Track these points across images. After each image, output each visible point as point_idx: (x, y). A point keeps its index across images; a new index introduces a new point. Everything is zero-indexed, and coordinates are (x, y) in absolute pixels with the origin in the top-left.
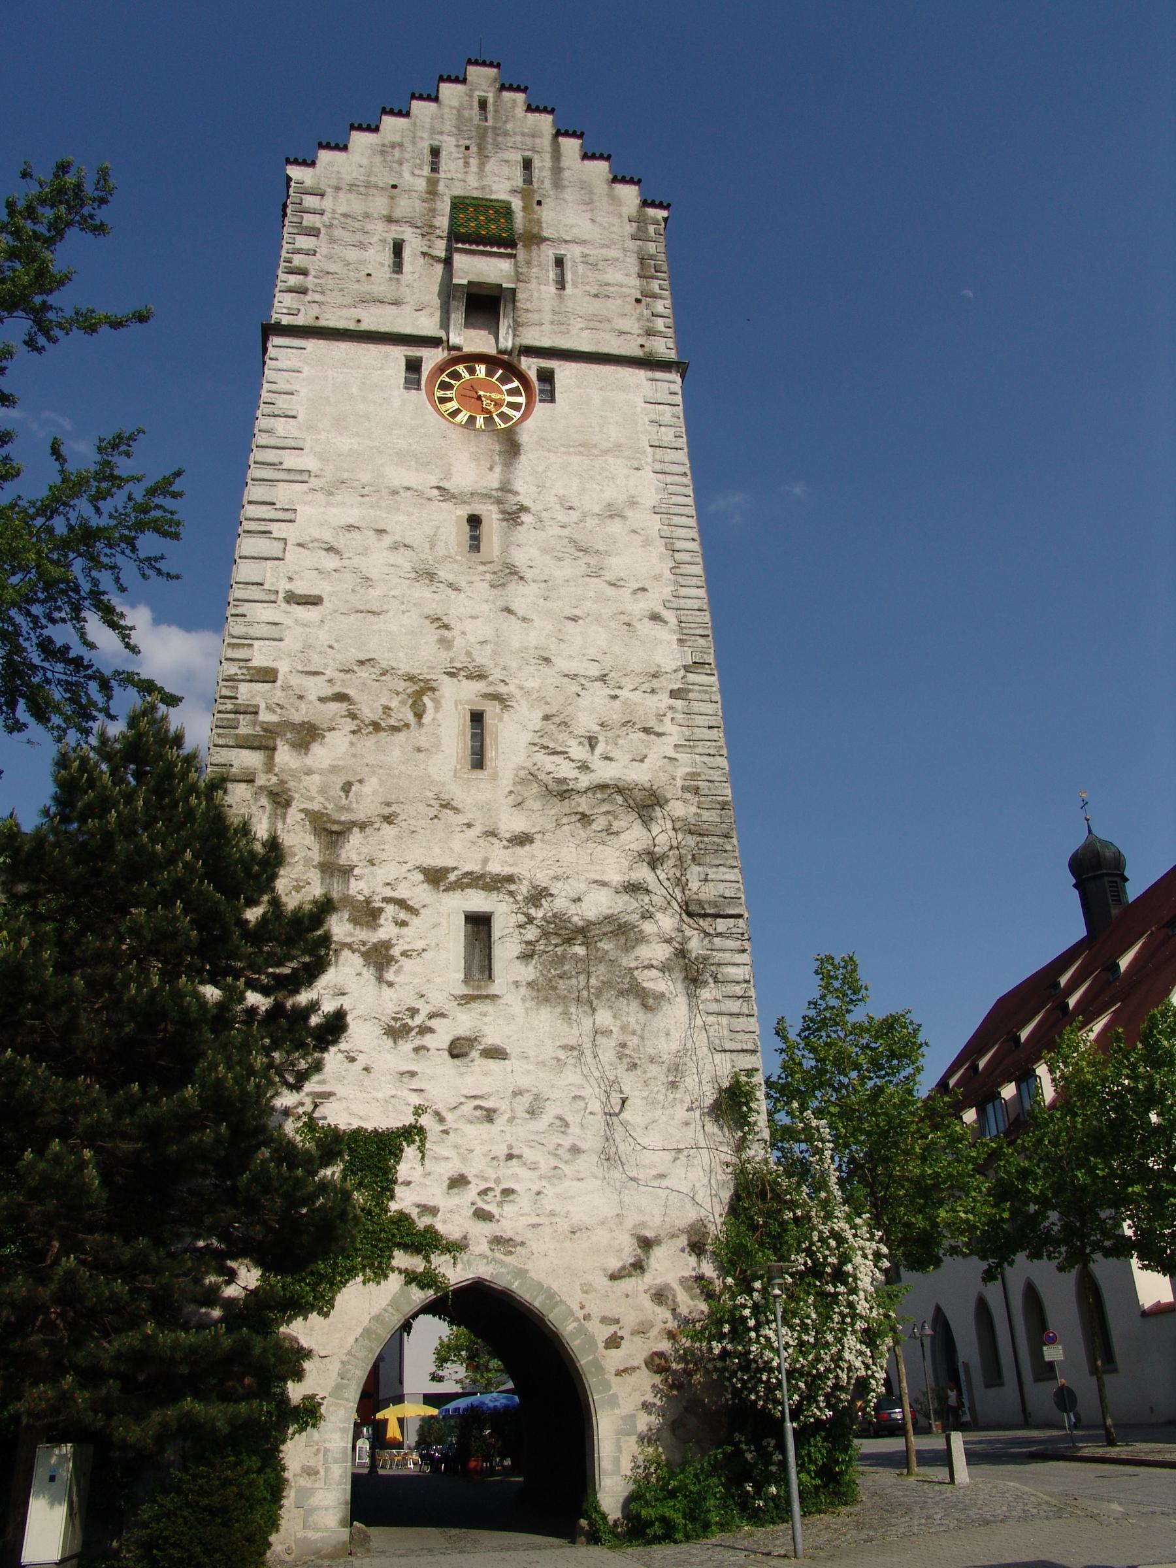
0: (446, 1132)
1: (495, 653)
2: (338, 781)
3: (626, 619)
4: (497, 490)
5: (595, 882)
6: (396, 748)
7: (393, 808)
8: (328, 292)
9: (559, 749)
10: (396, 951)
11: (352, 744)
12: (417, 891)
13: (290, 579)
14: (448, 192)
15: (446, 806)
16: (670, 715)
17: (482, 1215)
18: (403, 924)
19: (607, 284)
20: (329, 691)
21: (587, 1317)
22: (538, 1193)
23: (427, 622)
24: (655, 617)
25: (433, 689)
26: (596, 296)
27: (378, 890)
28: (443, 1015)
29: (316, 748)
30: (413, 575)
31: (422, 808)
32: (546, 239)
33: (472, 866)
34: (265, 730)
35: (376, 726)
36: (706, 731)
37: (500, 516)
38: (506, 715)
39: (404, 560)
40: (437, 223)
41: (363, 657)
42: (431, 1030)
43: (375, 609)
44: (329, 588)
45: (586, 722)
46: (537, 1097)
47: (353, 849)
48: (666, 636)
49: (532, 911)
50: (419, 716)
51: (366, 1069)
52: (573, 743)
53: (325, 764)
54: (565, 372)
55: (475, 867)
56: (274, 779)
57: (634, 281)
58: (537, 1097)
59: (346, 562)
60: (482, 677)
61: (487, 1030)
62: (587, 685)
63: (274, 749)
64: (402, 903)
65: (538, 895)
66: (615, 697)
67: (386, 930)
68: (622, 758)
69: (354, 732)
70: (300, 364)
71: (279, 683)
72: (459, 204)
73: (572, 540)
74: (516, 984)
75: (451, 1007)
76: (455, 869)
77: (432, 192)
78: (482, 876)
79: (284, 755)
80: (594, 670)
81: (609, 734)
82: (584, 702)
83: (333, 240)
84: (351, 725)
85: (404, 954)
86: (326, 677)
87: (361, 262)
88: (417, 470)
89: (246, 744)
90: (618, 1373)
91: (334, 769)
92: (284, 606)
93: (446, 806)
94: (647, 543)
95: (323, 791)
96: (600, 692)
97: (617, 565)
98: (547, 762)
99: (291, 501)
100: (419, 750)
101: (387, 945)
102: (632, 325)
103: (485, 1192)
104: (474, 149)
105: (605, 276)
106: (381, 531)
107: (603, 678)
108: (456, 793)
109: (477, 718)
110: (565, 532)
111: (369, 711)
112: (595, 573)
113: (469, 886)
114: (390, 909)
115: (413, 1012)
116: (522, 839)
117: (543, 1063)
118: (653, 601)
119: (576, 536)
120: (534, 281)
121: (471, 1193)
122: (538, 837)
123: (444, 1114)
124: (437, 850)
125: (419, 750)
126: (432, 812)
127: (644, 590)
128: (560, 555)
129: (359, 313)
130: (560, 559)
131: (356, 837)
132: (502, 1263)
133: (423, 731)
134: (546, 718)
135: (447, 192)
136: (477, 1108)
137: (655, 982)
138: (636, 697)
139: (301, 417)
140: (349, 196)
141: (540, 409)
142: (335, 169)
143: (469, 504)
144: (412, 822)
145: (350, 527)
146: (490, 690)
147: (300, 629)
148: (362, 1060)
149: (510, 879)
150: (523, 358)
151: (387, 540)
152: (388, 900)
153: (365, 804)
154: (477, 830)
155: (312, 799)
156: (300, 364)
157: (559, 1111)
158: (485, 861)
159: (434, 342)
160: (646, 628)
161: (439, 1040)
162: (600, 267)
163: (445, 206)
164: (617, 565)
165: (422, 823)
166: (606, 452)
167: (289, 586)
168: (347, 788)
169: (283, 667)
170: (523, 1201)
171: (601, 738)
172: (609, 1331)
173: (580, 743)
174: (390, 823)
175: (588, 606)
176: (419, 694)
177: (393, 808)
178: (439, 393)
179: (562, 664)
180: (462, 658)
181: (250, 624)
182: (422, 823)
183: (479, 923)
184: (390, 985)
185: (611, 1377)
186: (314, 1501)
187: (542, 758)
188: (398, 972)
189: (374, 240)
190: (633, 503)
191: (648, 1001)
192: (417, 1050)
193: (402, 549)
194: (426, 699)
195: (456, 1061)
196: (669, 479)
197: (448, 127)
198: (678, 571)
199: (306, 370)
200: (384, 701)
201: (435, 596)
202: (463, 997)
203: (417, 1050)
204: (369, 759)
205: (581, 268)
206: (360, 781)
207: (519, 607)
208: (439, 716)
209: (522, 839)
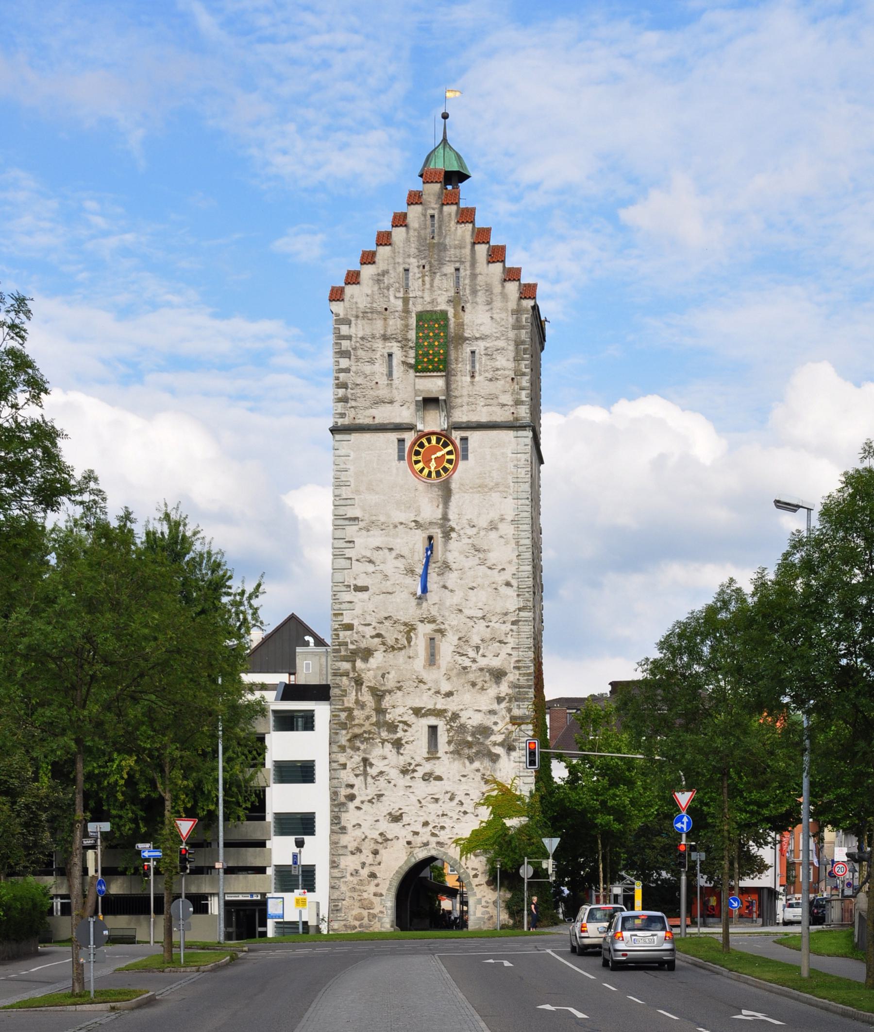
0: (421, 807)
1: (439, 609)
2: (380, 673)
3: (494, 586)
4: (440, 519)
5: (476, 710)
6: (401, 656)
7: (401, 684)
8: (358, 399)
9: (465, 653)
10: (403, 742)
11: (384, 656)
12: (410, 718)
13: (355, 579)
14: (416, 308)
15: (421, 681)
16: (511, 633)
17: (433, 835)
18: (406, 731)
19: (498, 369)
20: (374, 633)
21: (467, 868)
22: (453, 827)
23: (411, 596)
24: (508, 584)
25: (415, 629)
26: (491, 380)
27: (397, 718)
28: (421, 765)
29: (371, 660)
30: (405, 572)
31: (411, 682)
32: (467, 339)
33: (430, 706)
34: (351, 653)
35: (392, 647)
36: (526, 640)
37: (441, 535)
38: (443, 639)
39: (400, 563)
40: (409, 337)
41: (386, 616)
42: (416, 771)
43: (391, 591)
44: (371, 582)
45: (475, 640)
46: (453, 794)
47: (387, 702)
48: (511, 592)
49: (452, 724)
50: (409, 642)
51: (395, 785)
52: (470, 650)
53: (374, 666)
54: (474, 437)
55: (431, 706)
56: (356, 674)
57: (511, 365)
58: (453, 794)
59: (377, 568)
60: (434, 621)
61: (436, 770)
62: (477, 621)
63: (355, 661)
64: (405, 723)
65: (455, 716)
66: (488, 627)
67: (400, 734)
68: (490, 655)
69: (384, 651)
70: (349, 451)
71: (355, 630)
72: (420, 316)
73: (473, 545)
74: (446, 753)
75: (423, 762)
76: (424, 708)
77: (406, 311)
78: (434, 710)
79: (359, 664)
80: (480, 614)
81: (485, 645)
82: (474, 630)
83: (358, 360)
84: (383, 648)
85: (406, 743)
86: (372, 626)
87: (373, 374)
88: (405, 512)
89: (345, 659)
90: (477, 886)
91: (378, 668)
92: (353, 592)
93: (421, 681)
94: (507, 543)
95: (375, 677)
96: (483, 623)
97: (493, 557)
98: (460, 659)
99: (352, 537)
100: (410, 657)
101: (400, 739)
102: (507, 399)
103: (434, 827)
104: (427, 268)
105: (497, 363)
106: (391, 549)
107: (483, 618)
108: (425, 675)
109: (432, 639)
110: (470, 541)
111: (390, 642)
112: (482, 563)
113: (430, 715)
114: (401, 725)
115: (410, 764)
116: (449, 694)
117: (454, 782)
118: (507, 576)
119: (475, 543)
120: (459, 374)
121: (430, 827)
122: (455, 693)
123: (421, 800)
124: (417, 701)
125: (410, 657)
126: (415, 685)
127: (504, 569)
128: (467, 554)
129: (373, 412)
130: (467, 557)
131: (387, 698)
132: (440, 851)
133: (412, 648)
134: (460, 639)
135: (414, 308)
136: (432, 798)
137: (498, 750)
138: (497, 625)
139: (352, 485)
140: (363, 321)
141: (462, 464)
142: (355, 300)
143: (427, 529)
144: (408, 689)
145: (378, 548)
146: (437, 627)
147: (361, 604)
148: (393, 782)
149: (445, 711)
150: (453, 432)
151: (394, 554)
152: (400, 722)
153: (390, 682)
154: (433, 691)
155: (370, 681)
156: (349, 451)
157: (460, 799)
158: (435, 704)
159: (410, 428)
160: (504, 590)
161: (419, 774)
162: (494, 356)
163: (413, 321)
164: (493, 557)
165: (412, 689)
166: (491, 489)
167: (355, 582)
168: (383, 676)
169: (356, 623)
170: (447, 830)
171: (482, 647)
172: (474, 872)
173: (473, 650)
174: (400, 690)
175: (479, 581)
176: (408, 632)
177: (401, 684)
178: (414, 458)
179: (467, 612)
180: (426, 613)
181: (341, 603)
182: (412, 689)
183: (433, 729)
184: (402, 754)
185: (474, 886)
186: (383, 920)
187: (457, 657)
188: (404, 750)
189: (378, 356)
190: (502, 520)
191: (495, 758)
192: (411, 778)
193: (400, 558)
194: (412, 634)
195: (425, 782)
196: (520, 502)
197: (413, 251)
198: (519, 557)
199: (352, 454)
200: (395, 636)
201: (413, 582)
202: (427, 758)
203: (411, 778)
204: (391, 663)
205: (484, 358)
206: (388, 673)
207: (450, 585)
208: (417, 641)
209: (449, 694)
